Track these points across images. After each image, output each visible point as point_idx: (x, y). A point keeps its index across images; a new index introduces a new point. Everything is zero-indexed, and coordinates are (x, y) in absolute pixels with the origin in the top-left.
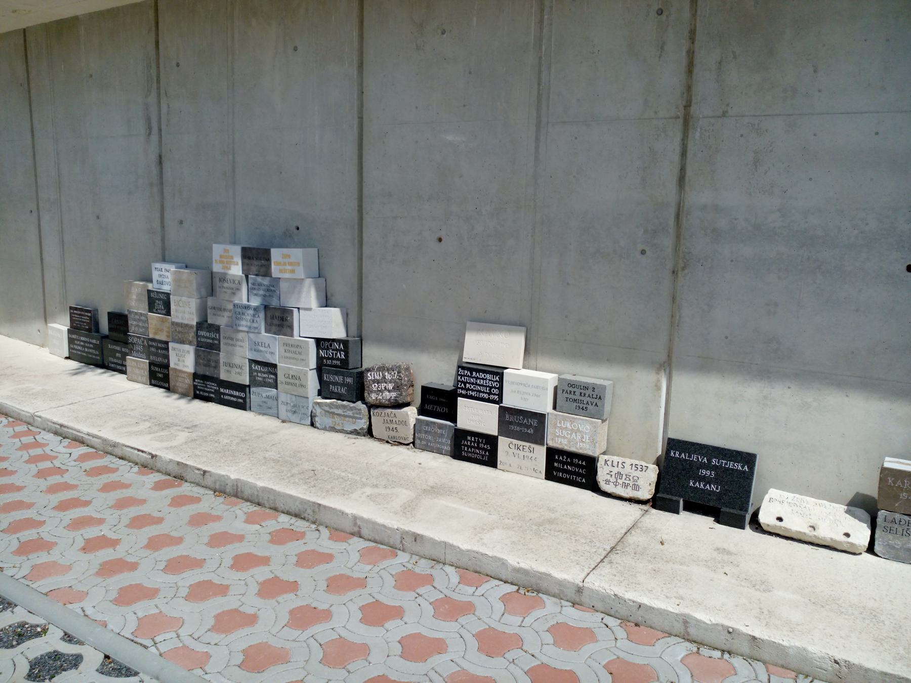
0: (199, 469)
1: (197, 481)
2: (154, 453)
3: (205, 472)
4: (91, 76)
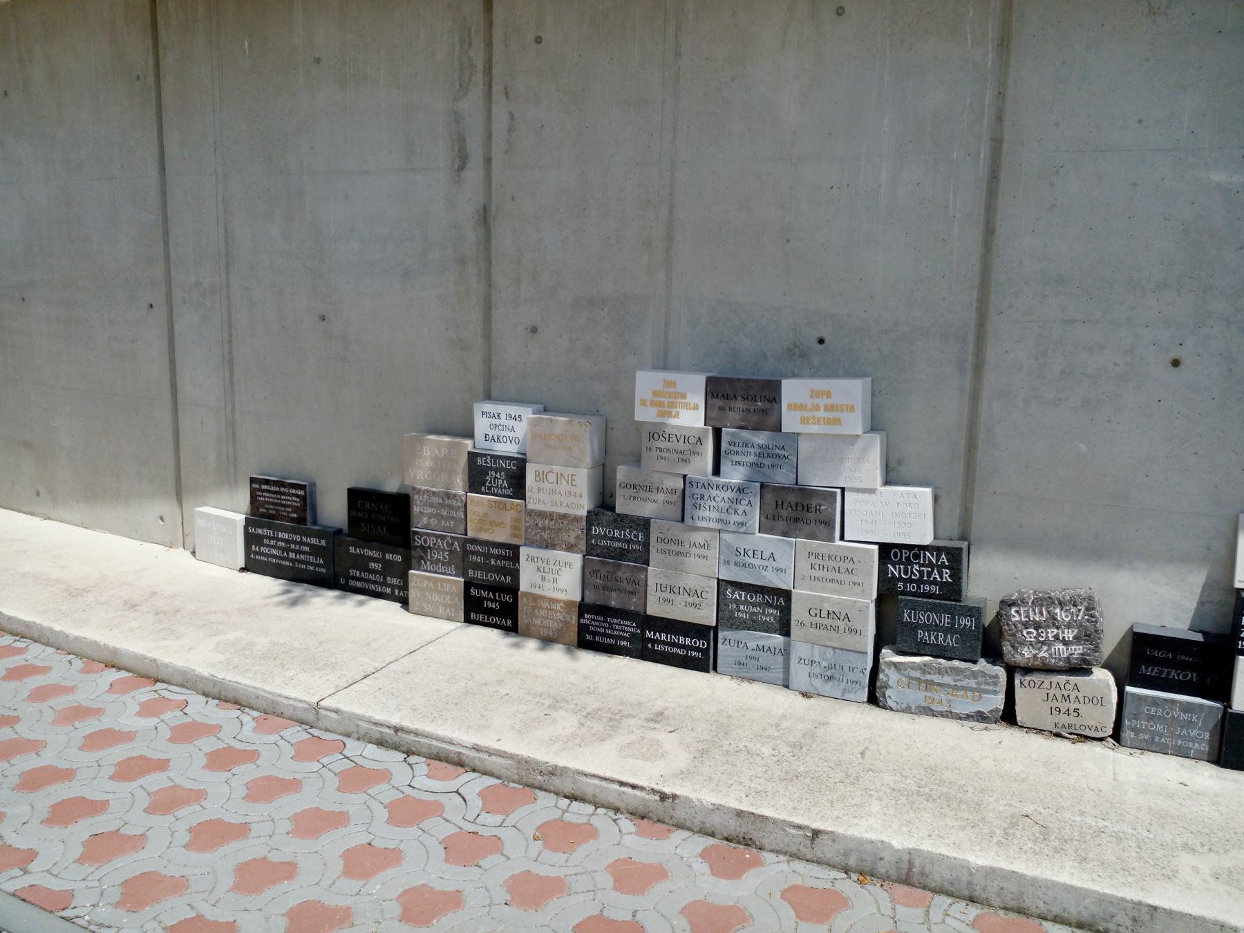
0: (799, 827)
1: (793, 849)
2: (667, 790)
3: (816, 833)
4: (318, 61)
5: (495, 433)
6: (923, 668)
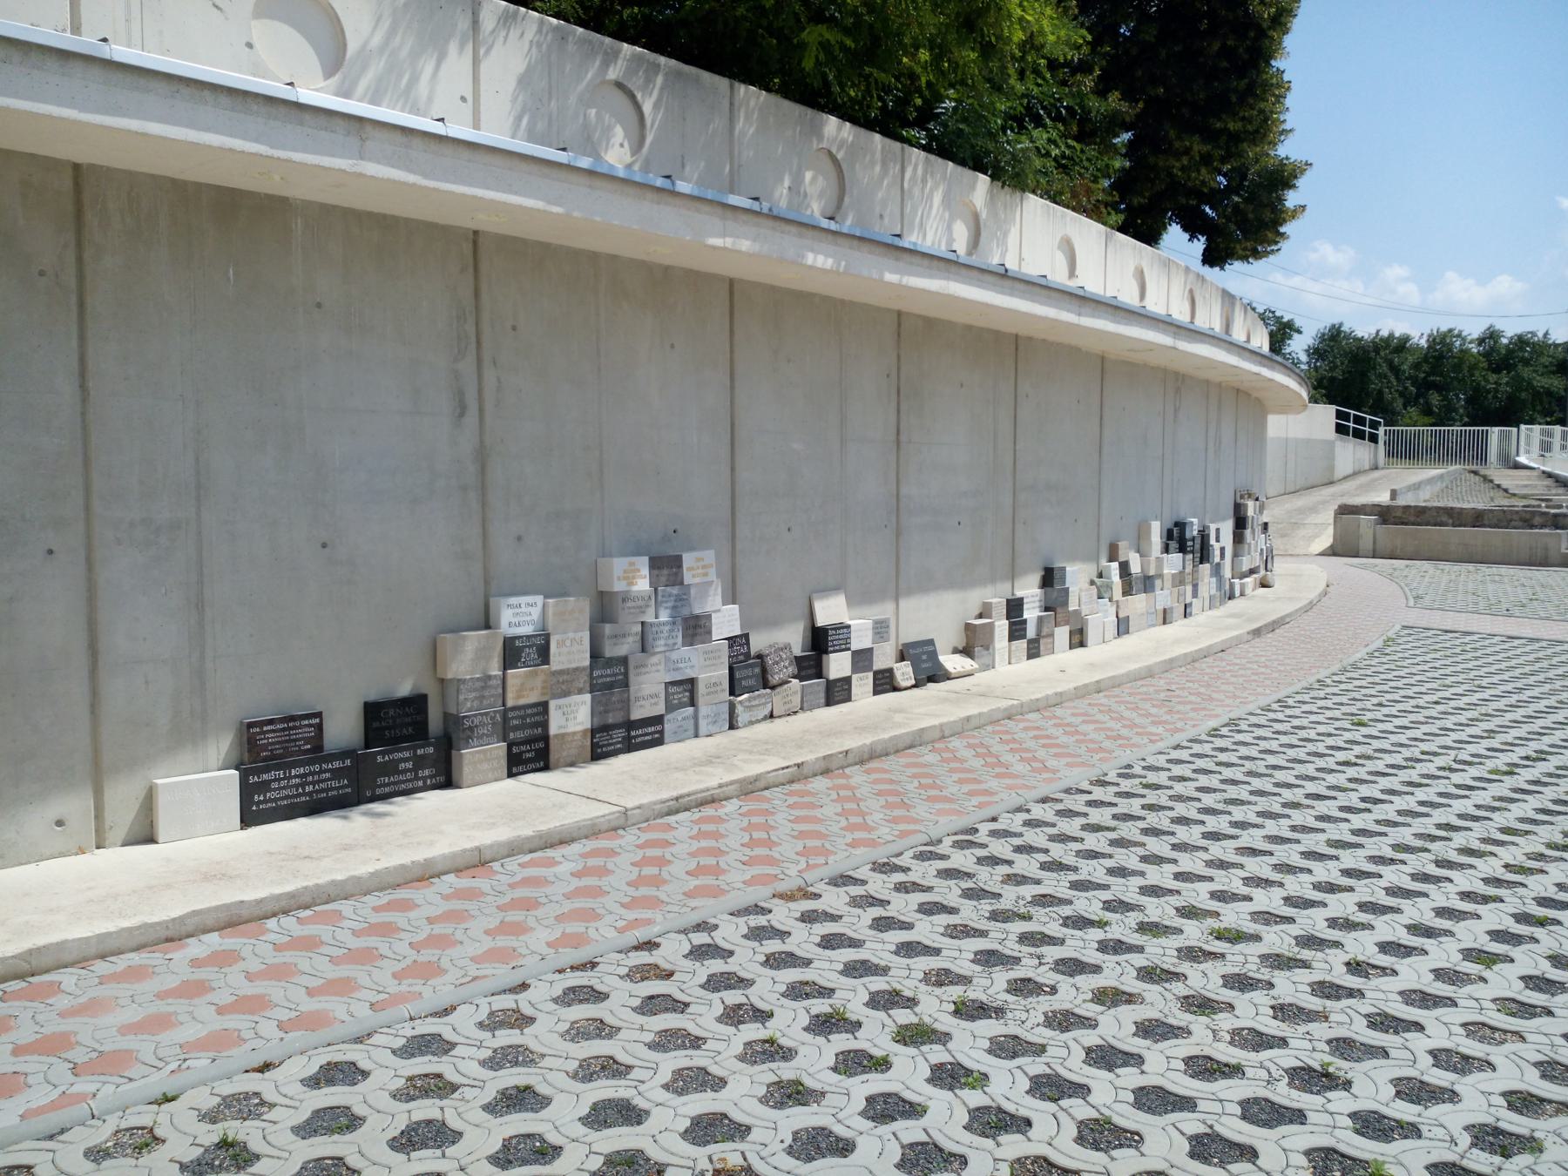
5: (516, 620)
6: (749, 700)
